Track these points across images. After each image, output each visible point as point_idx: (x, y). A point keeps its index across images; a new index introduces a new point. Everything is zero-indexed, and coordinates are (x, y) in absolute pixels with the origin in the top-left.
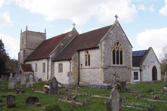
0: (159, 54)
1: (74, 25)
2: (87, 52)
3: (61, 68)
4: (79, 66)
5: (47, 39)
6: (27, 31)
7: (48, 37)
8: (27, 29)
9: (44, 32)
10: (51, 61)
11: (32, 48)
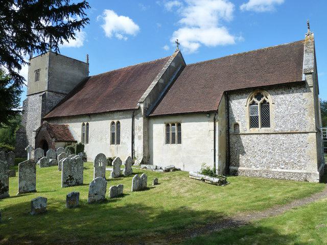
3: (176, 134)
4: (229, 128)
5: (89, 75)
7: (93, 72)
9: (86, 62)
11: (60, 91)
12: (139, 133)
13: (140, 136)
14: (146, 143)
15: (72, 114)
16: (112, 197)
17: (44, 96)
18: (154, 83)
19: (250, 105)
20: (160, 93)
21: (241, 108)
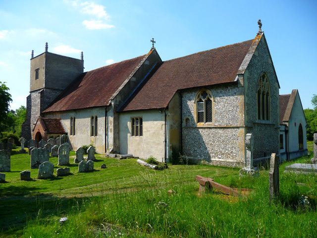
0: (307, 104)
1: (153, 42)
2: (202, 95)
3: (139, 128)
4: (182, 122)
5: (85, 71)
6: (46, 52)
7: (88, 68)
8: (47, 48)
9: (80, 58)
10: (114, 114)
11: (57, 88)
12: (111, 127)
13: (112, 129)
14: (117, 135)
15: (62, 109)
16: (58, 175)
17: (41, 93)
18: (126, 81)
19: (198, 102)
20: (132, 90)
21: (192, 105)
